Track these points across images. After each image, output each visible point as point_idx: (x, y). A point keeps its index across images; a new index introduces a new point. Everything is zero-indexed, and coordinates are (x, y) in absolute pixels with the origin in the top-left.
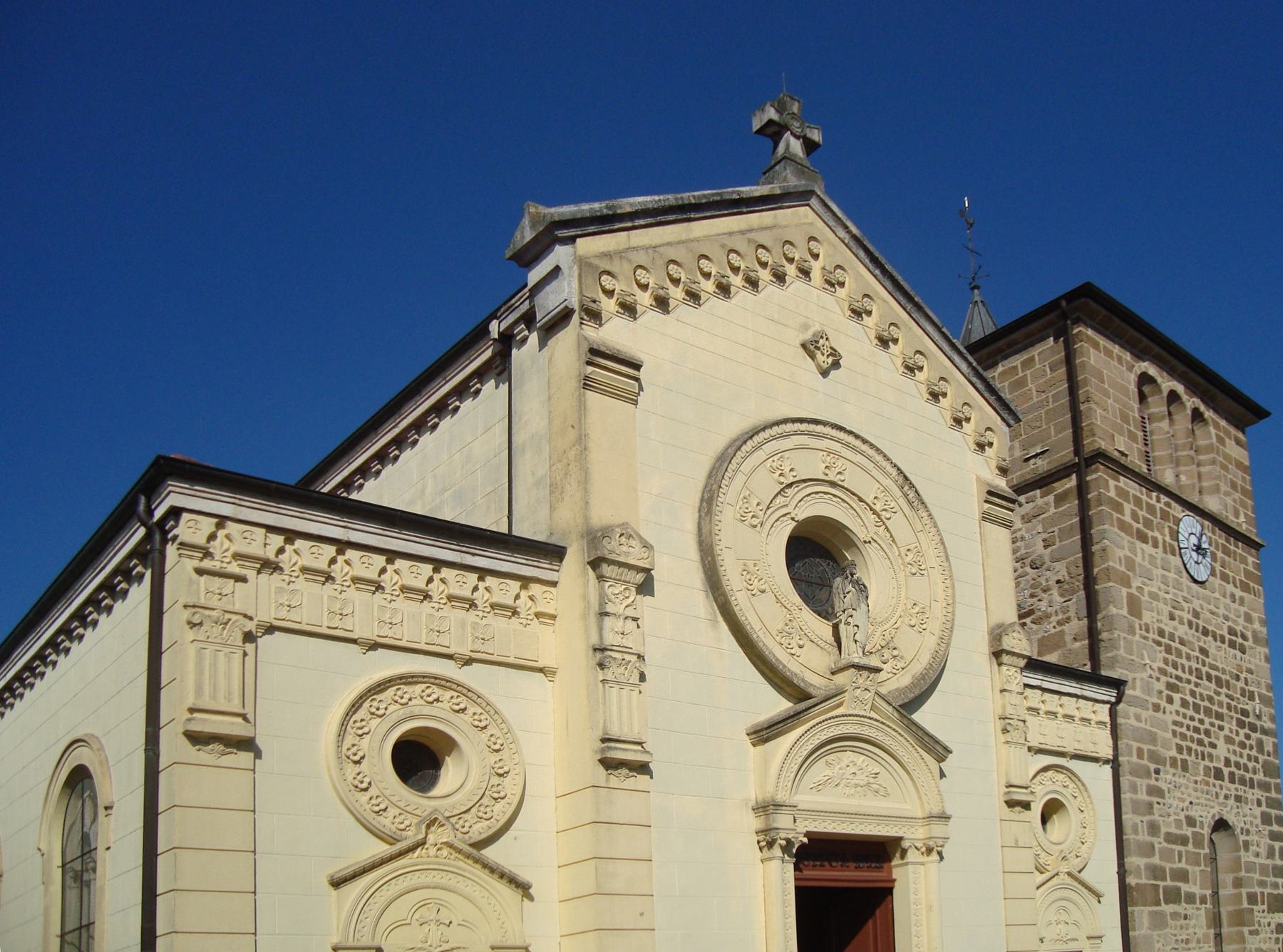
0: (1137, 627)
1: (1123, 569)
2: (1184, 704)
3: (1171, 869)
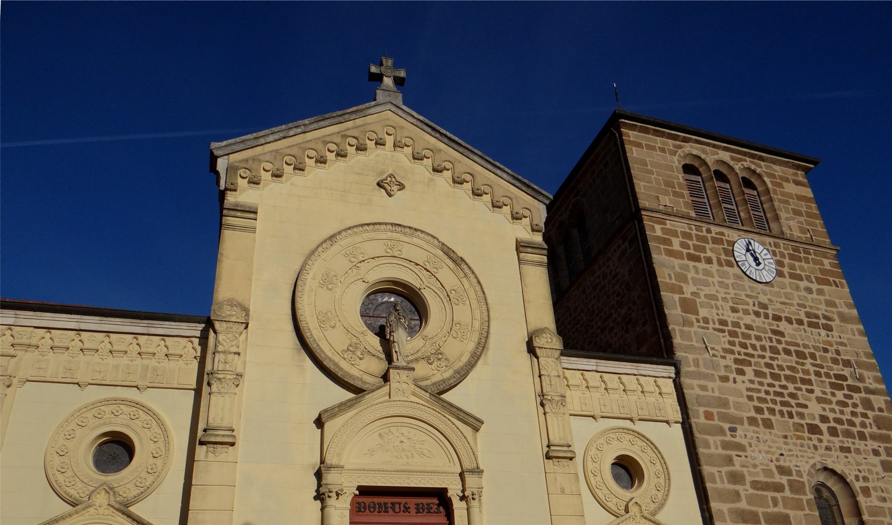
0: (695, 321)
1: (673, 281)
2: (758, 373)
3: (764, 513)
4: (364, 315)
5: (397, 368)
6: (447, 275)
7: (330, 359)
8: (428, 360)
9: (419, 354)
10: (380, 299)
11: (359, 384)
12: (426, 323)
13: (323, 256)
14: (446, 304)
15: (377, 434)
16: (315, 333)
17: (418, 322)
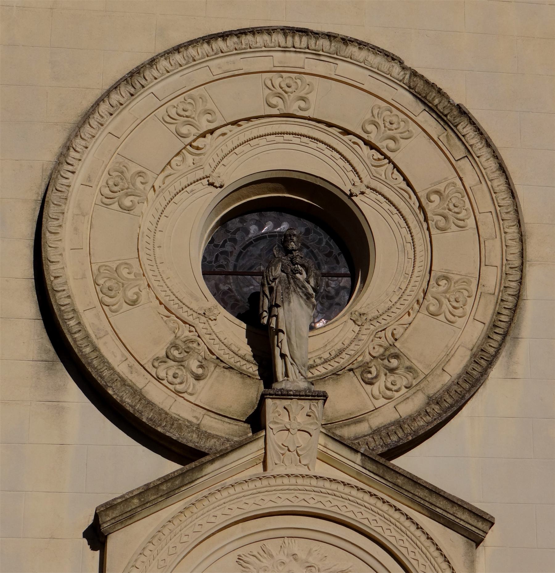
4: (213, 268)
5: (284, 395)
6: (422, 155)
7: (124, 382)
8: (364, 373)
9: (344, 360)
10: (253, 229)
11: (191, 439)
12: (364, 281)
13: (112, 125)
14: (416, 230)
15: (233, 557)
16: (88, 319)
17: (345, 282)
